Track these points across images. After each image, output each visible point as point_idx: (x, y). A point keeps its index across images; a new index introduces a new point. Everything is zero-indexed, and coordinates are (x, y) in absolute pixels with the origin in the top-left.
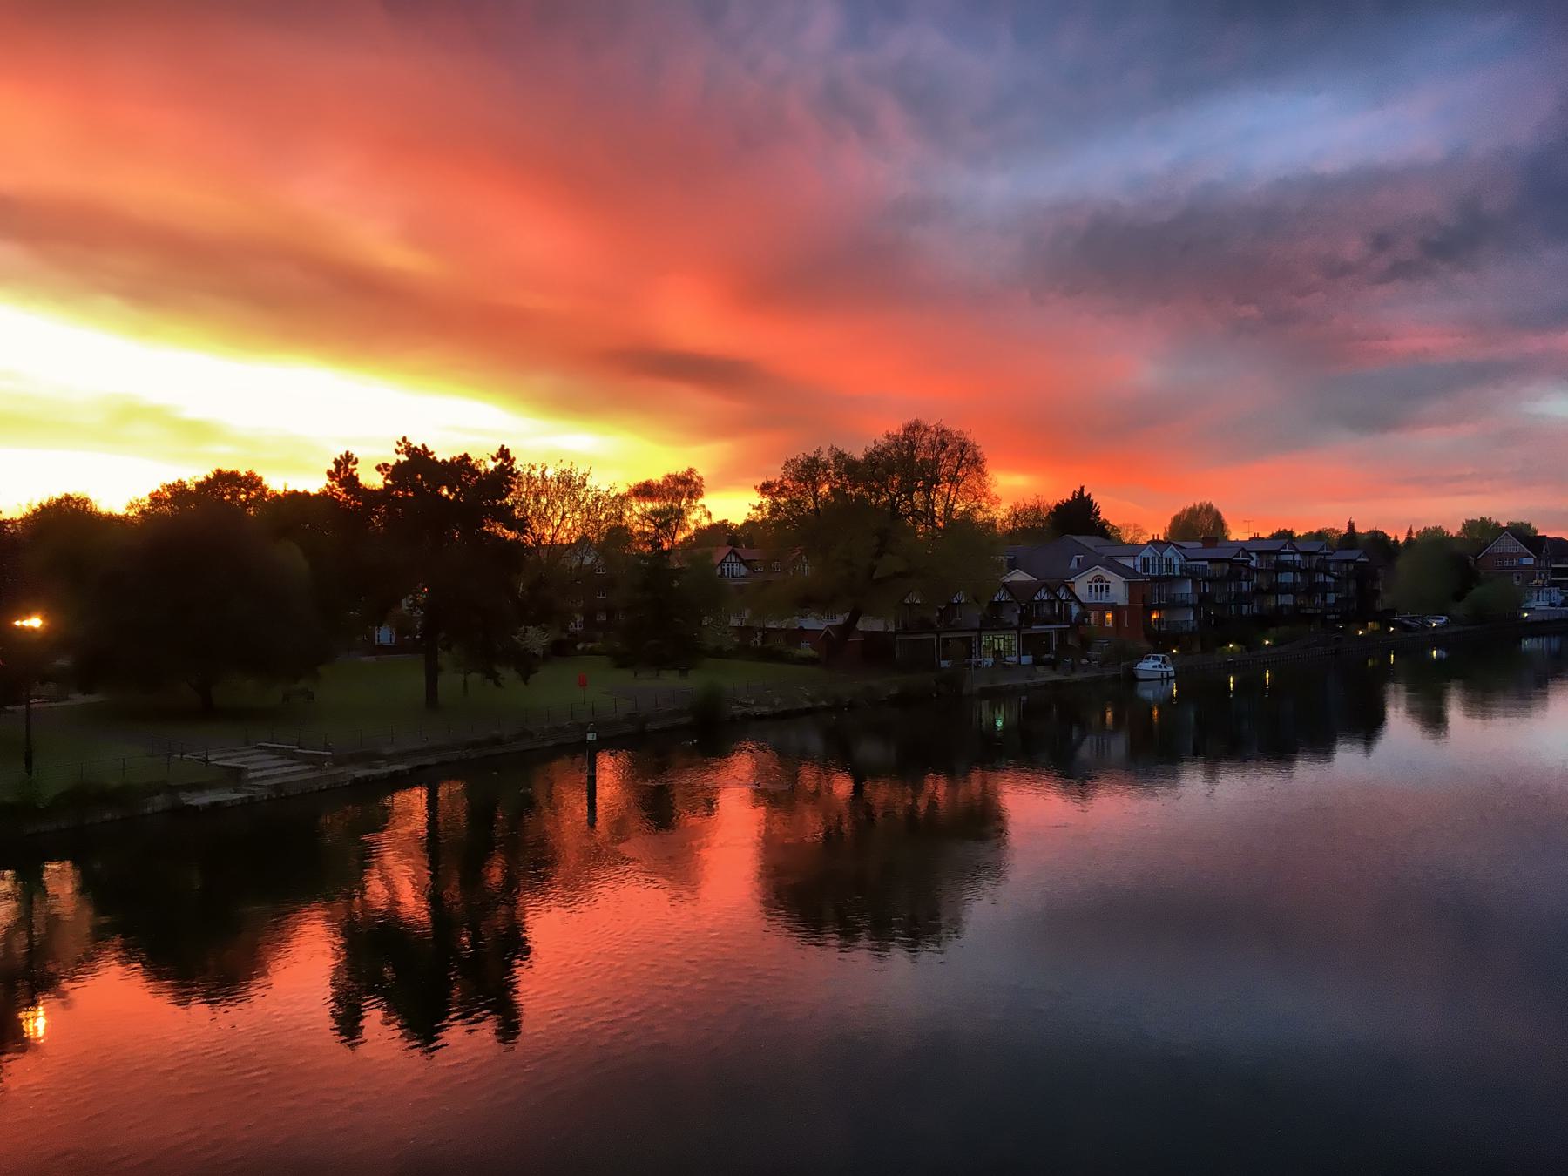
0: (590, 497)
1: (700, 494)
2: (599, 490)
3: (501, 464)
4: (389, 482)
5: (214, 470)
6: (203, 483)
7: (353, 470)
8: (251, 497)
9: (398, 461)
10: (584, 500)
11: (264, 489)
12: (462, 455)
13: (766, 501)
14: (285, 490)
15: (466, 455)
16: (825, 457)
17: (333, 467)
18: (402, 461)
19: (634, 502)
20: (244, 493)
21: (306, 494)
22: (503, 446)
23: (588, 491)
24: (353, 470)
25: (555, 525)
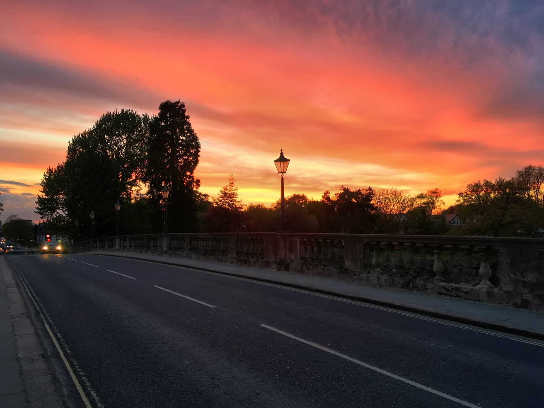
0: (402, 199)
1: (440, 196)
2: (405, 197)
3: (369, 192)
4: (338, 198)
5: (293, 194)
6: (290, 198)
7: (329, 195)
8: (303, 202)
9: (341, 192)
10: (401, 200)
11: (307, 199)
12: (358, 189)
13: (461, 198)
14: (312, 200)
15: (360, 189)
16: (482, 183)
17: (323, 195)
18: (342, 192)
19: (417, 200)
20: (301, 201)
21: (318, 202)
22: (370, 187)
23: (402, 197)
24: (329, 195)
25: (391, 208)
